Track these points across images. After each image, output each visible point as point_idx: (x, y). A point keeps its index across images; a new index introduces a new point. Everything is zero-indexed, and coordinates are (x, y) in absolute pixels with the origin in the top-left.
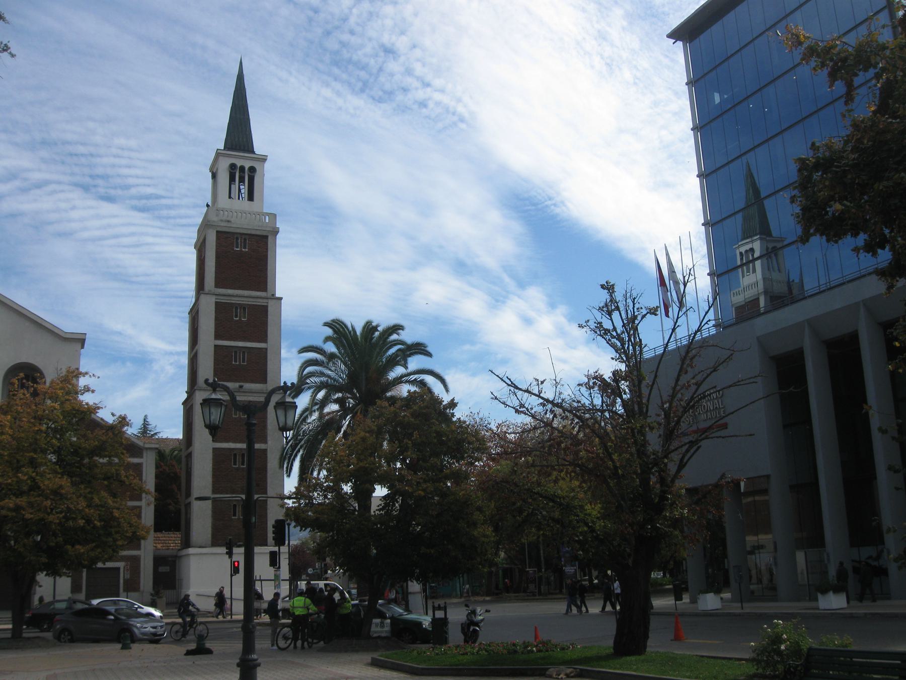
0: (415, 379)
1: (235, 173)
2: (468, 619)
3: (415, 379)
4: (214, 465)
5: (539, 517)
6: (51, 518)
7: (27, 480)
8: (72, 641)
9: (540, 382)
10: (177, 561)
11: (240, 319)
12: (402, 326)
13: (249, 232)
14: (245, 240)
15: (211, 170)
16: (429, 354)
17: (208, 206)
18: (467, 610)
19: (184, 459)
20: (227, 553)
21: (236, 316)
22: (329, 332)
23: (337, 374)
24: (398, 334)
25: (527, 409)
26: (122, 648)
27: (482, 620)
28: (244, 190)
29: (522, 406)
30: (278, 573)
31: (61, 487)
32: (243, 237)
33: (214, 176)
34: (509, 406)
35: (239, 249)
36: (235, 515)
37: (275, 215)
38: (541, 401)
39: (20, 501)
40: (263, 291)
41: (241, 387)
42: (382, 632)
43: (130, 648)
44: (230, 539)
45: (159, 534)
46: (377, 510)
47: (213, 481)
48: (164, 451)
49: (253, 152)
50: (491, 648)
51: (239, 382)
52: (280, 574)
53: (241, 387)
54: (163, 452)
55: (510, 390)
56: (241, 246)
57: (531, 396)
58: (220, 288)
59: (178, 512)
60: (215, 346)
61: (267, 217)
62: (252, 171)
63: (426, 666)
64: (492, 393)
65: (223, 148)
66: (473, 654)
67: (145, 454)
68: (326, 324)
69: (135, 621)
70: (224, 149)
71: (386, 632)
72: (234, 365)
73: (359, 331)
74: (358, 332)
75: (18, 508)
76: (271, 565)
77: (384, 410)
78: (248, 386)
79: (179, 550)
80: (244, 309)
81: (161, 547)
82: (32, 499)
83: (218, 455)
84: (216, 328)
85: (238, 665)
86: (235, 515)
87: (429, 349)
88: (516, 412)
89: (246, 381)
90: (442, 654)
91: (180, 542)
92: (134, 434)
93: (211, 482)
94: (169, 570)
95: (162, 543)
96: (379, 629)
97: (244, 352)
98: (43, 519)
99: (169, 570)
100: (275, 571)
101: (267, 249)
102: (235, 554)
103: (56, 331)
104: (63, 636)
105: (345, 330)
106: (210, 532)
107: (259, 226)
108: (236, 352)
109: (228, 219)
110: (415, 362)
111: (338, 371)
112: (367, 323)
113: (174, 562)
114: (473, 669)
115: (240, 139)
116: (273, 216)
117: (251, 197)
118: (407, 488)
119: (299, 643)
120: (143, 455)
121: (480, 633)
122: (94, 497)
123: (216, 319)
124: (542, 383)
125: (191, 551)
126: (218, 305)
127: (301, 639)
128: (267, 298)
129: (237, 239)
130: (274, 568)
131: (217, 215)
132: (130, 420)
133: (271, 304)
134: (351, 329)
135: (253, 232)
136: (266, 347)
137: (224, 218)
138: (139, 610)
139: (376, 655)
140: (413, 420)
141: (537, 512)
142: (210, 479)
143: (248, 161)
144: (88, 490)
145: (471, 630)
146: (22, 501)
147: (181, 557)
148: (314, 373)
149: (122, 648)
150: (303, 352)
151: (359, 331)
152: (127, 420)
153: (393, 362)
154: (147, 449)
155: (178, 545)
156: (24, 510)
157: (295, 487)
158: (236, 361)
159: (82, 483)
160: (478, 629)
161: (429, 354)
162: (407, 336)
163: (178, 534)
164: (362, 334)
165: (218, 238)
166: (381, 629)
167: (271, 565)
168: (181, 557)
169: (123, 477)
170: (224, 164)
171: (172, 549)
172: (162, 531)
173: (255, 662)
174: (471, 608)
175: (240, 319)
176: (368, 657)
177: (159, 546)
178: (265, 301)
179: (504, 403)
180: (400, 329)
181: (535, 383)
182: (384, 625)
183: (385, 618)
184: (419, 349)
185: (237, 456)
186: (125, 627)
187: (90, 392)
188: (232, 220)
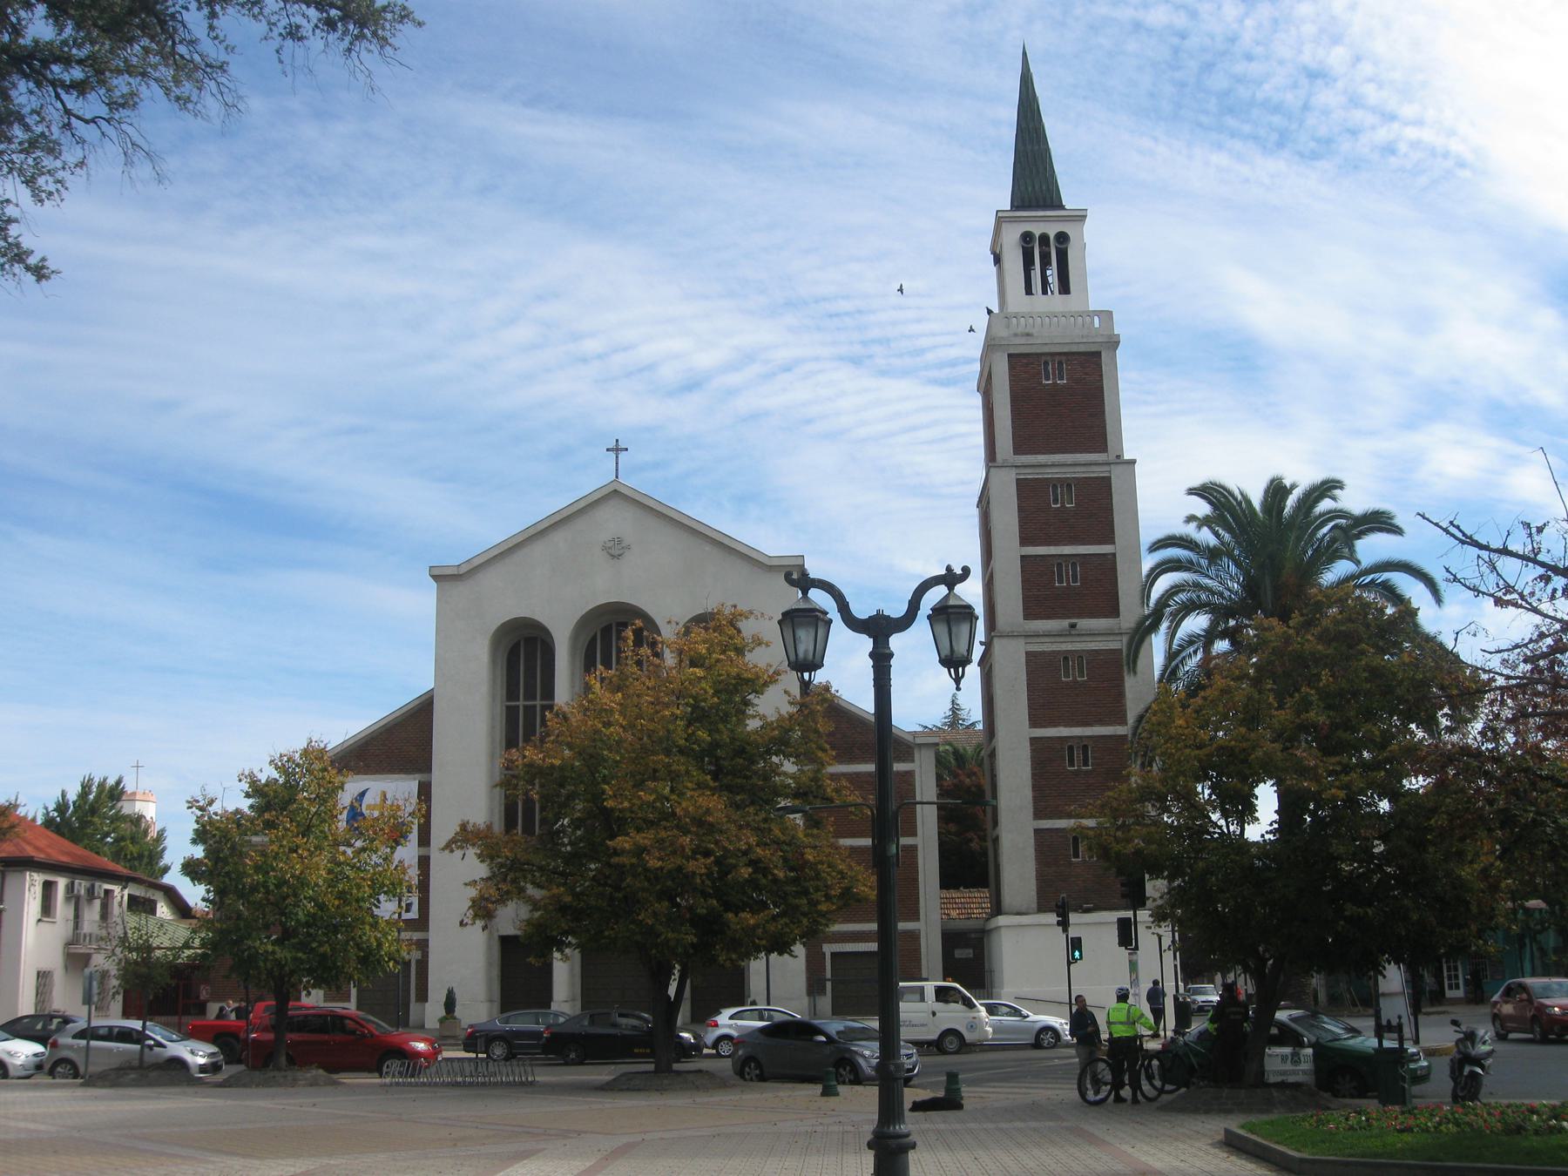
0: (1372, 579)
1: (1033, 248)
2: (1459, 1052)
3: (1373, 581)
4: (1033, 768)
5: (1548, 830)
6: (691, 866)
7: (654, 801)
8: (762, 1078)
9: (1534, 530)
10: (985, 940)
11: (1063, 505)
12: (1339, 482)
13: (1066, 350)
14: (1060, 363)
15: (994, 253)
16: (1397, 531)
17: (990, 312)
18: (1456, 1031)
19: (986, 762)
20: (1059, 923)
21: (1056, 501)
22: (1202, 508)
23: (1221, 584)
24: (1334, 499)
25: (1522, 596)
26: (823, 1094)
27: (1490, 1054)
28: (1052, 274)
29: (1509, 589)
30: (1134, 957)
31: (708, 812)
32: (1057, 359)
33: (998, 260)
34: (1484, 593)
35: (1050, 382)
36: (1076, 856)
37: (1110, 313)
38: (1541, 571)
39: (644, 838)
40: (1100, 452)
41: (1073, 626)
42: (1294, 1073)
43: (837, 1094)
44: (1063, 898)
45: (953, 893)
46: (1267, 832)
47: (1034, 797)
48: (965, 749)
49: (1061, 207)
50: (1467, 1119)
51: (1069, 618)
52: (1137, 961)
53: (1073, 626)
54: (962, 751)
55: (1479, 557)
56: (1054, 374)
57: (1527, 566)
58: (1023, 454)
59: (985, 853)
60: (1022, 557)
61: (1096, 319)
62: (1062, 240)
63: (1313, 1154)
64: (1447, 570)
65: (1009, 209)
66: (1427, 1130)
67: (917, 756)
68: (1192, 492)
69: (858, 1045)
70: (1011, 210)
71: (1304, 1072)
72: (1057, 588)
73: (1256, 499)
74: (1257, 504)
75: (640, 851)
76: (1121, 944)
77: (1267, 634)
78: (1085, 624)
79: (988, 919)
80: (1069, 486)
81: (959, 914)
82: (663, 834)
83: (1039, 748)
84: (1021, 527)
85: (870, 1145)
86: (1076, 856)
87: (1398, 521)
88: (1496, 605)
89: (1080, 616)
90: (1360, 1128)
91: (989, 905)
92: (937, 727)
93: (1031, 798)
94: (971, 956)
95: (959, 909)
96: (1289, 1067)
97: (1074, 565)
98: (680, 869)
99: (971, 956)
100: (1130, 954)
101: (1101, 376)
102: (1073, 924)
103: (754, 555)
104: (747, 1069)
105: (1229, 499)
106: (1034, 888)
107: (1082, 336)
108: (1059, 565)
109: (1027, 331)
110: (1372, 548)
111: (1228, 582)
112: (1272, 481)
113: (981, 940)
114: (1409, 1167)
115: (1037, 188)
116: (1107, 316)
117: (1065, 288)
118: (1306, 784)
119: (1126, 1092)
120: (913, 757)
121: (1486, 1081)
122: (773, 828)
123: (1021, 509)
124: (1540, 530)
125: (1002, 920)
126: (1020, 483)
127: (1130, 1085)
128: (1109, 464)
129: (1046, 363)
130: (1126, 948)
131: (1008, 327)
132: (837, 692)
133: (1116, 475)
134: (1239, 497)
135: (1074, 349)
136: (1113, 551)
137: (1020, 330)
138: (157, 1049)
139: (1234, 1124)
140: (1320, 647)
141: (1544, 818)
142: (1028, 793)
143: (1052, 224)
144: (763, 815)
145: (1465, 1073)
146: (644, 839)
147: (990, 931)
148: (1184, 586)
149: (823, 1094)
150: (1155, 550)
151: (1256, 499)
152: (833, 691)
153: (1329, 554)
154: (920, 746)
155: (987, 910)
156: (649, 853)
157: (1276, 812)
158: (1061, 581)
159: (752, 803)
160: (1480, 1071)
161: (1397, 531)
162: (1354, 501)
163: (986, 893)
164: (1265, 503)
165: (1012, 367)
166: (1294, 1068)
167: (1121, 944)
168: (990, 931)
169: (829, 790)
170: (1012, 236)
171: (977, 918)
172: (960, 886)
173: (906, 1140)
174: (1464, 1028)
175: (1063, 505)
176: (1217, 1126)
177: (954, 914)
178: (1106, 468)
179: (1474, 589)
180: (1336, 488)
181: (1523, 533)
182: (1299, 1059)
183: (1301, 1045)
184: (1378, 521)
185: (1090, 749)
186: (847, 1055)
187: (763, 645)
188: (1034, 331)
